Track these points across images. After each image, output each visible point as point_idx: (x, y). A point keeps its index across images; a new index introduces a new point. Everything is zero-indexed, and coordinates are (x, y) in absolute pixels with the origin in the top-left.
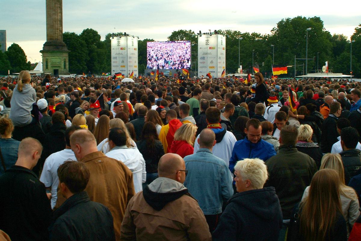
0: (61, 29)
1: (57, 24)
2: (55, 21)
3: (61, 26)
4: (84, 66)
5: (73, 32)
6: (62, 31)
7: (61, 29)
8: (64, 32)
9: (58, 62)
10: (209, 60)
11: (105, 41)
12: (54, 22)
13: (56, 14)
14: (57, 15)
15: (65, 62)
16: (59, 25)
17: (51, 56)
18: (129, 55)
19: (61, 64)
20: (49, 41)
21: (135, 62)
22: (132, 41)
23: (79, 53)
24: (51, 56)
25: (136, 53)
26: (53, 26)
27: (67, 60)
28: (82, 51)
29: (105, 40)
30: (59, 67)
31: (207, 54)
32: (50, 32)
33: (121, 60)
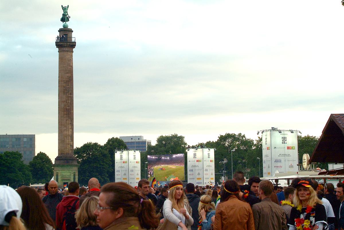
0: (72, 144)
1: (68, 139)
2: (66, 137)
3: (72, 141)
4: (106, 179)
5: (95, 143)
6: (73, 146)
7: (72, 144)
8: (75, 147)
9: (68, 176)
10: (197, 172)
11: (156, 145)
12: (65, 138)
13: (67, 130)
14: (68, 131)
15: (74, 175)
16: (69, 140)
17: (61, 169)
18: (130, 168)
19: (71, 177)
20: (60, 155)
21: (138, 174)
22: (120, 155)
23: (100, 164)
24: (61, 169)
25: (139, 166)
26: (64, 141)
27: (77, 174)
28: (103, 162)
29: (157, 144)
30: (69, 180)
31: (195, 166)
32: (61, 147)
33: (123, 173)
